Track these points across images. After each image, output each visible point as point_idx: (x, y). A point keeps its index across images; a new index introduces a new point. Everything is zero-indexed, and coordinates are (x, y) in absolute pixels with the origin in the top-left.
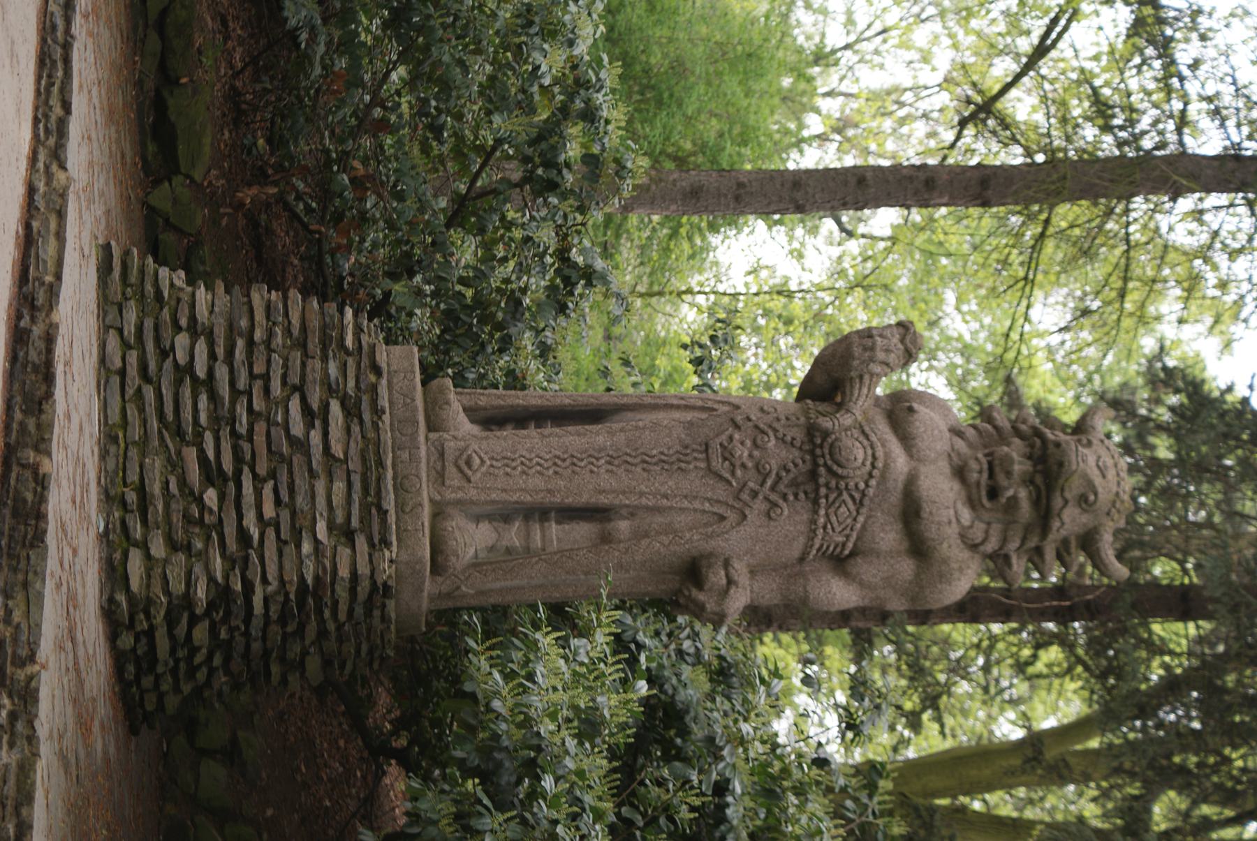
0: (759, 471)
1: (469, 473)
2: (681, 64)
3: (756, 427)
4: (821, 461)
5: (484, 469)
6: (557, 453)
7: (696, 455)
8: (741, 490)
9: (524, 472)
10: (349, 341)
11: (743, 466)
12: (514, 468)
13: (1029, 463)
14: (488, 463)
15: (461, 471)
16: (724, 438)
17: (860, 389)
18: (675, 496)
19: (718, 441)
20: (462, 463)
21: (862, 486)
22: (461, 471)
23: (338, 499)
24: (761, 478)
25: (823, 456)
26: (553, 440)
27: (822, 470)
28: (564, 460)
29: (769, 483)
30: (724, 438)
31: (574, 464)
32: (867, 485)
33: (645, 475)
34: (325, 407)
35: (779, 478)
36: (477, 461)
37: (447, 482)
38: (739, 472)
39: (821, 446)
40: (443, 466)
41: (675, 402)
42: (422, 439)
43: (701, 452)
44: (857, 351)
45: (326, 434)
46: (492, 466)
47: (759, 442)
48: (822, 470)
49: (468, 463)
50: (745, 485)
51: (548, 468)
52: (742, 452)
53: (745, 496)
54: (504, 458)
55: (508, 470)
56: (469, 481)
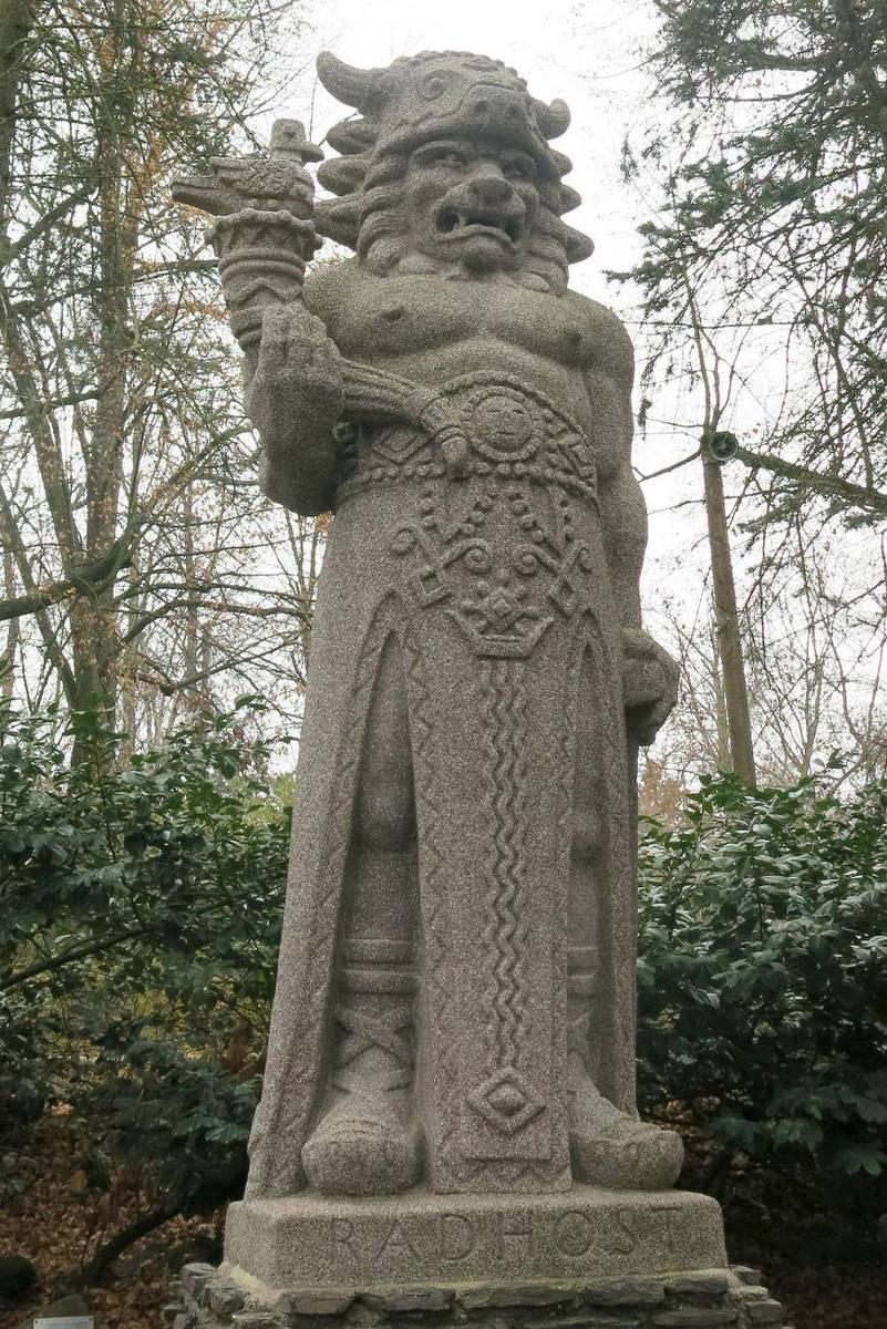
0: (531, 575)
3: (447, 566)
5: (522, 1079)
7: (501, 679)
8: (560, 611)
9: (524, 1001)
11: (522, 598)
12: (518, 1018)
13: (275, 137)
14: (509, 1070)
16: (472, 627)
17: (370, 385)
19: (477, 636)
20: (509, 1124)
24: (542, 573)
25: (513, 463)
26: (456, 939)
27: (533, 469)
28: (502, 921)
29: (549, 559)
30: (472, 627)
31: (510, 903)
32: (544, 404)
33: (530, 773)
35: (544, 542)
36: (506, 1092)
37: (545, 1153)
38: (532, 608)
39: (494, 463)
40: (511, 1160)
41: (362, 707)
42: (448, 1204)
43: (495, 668)
46: (514, 1063)
48: (533, 469)
49: (510, 1110)
50: (552, 601)
51: (517, 953)
52: (499, 598)
54: (498, 1038)
55: (521, 1029)
56: (542, 1110)
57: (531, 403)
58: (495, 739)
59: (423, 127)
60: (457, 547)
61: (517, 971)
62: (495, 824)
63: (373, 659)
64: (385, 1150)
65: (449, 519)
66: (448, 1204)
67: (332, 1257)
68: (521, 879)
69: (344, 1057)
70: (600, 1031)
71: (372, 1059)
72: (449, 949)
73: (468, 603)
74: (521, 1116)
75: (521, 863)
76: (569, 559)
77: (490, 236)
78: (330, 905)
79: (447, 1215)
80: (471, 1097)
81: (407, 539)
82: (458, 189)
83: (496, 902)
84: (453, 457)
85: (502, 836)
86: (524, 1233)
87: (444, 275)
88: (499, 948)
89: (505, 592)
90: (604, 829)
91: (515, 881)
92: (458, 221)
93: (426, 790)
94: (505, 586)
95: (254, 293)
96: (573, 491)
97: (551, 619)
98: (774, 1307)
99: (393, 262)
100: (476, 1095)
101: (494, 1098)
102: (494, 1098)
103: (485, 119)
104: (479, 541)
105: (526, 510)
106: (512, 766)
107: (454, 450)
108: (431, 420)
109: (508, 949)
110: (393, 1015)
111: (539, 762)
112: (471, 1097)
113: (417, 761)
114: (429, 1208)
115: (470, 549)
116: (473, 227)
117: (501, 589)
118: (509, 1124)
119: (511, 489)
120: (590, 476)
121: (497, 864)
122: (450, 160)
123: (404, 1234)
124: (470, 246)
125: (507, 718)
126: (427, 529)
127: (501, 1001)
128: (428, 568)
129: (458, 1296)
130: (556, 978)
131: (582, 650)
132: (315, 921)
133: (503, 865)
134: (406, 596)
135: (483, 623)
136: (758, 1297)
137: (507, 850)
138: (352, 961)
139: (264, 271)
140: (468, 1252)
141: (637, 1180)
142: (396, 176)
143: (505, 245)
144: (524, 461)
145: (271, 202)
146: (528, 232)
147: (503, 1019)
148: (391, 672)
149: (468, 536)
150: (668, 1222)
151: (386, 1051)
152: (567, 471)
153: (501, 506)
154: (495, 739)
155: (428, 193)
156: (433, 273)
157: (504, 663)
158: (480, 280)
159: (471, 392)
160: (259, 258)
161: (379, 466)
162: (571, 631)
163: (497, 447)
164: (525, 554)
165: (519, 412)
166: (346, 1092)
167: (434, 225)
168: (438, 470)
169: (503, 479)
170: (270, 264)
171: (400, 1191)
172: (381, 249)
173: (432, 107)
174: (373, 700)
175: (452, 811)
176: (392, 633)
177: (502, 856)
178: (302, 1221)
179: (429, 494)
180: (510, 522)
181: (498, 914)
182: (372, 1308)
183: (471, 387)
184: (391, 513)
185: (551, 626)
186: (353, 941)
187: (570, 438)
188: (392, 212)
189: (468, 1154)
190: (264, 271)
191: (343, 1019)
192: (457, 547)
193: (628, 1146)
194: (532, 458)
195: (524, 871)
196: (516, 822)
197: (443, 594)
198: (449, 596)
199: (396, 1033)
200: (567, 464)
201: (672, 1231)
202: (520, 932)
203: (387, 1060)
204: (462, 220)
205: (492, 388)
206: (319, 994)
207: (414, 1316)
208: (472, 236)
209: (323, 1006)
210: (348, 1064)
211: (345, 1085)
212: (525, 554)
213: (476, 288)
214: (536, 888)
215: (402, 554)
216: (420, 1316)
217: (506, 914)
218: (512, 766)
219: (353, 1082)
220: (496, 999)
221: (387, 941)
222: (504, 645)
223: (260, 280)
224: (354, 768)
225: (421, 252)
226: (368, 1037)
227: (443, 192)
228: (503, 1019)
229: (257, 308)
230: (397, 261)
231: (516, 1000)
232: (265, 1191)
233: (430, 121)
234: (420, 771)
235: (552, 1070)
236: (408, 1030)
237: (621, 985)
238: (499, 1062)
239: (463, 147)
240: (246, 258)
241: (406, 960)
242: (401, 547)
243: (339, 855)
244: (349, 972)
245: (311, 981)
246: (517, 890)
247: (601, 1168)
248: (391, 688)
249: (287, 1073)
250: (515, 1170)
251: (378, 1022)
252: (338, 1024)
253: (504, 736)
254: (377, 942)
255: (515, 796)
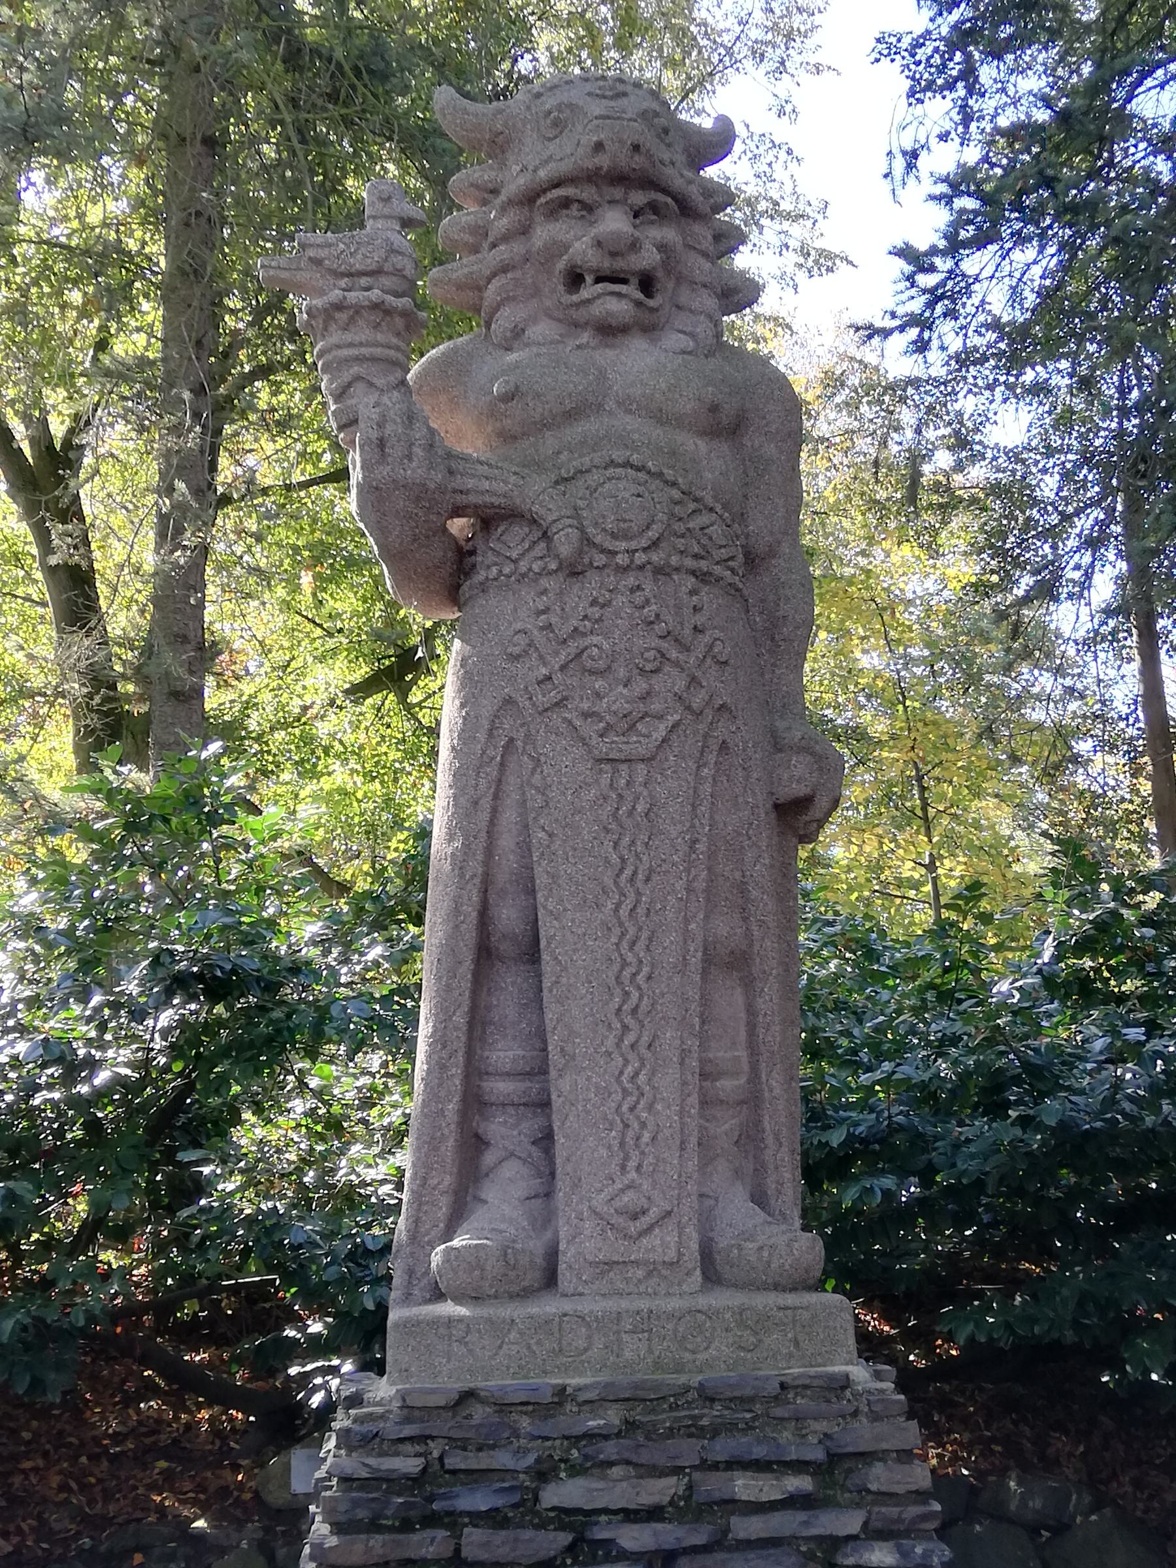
1: (654, 1213)
2: (509, 141)
3: (563, 668)
4: (640, 558)
6: (611, 1042)
9: (650, 1107)
10: (408, 1464)
11: (645, 697)
12: (643, 1125)
15: (650, 1229)
16: (589, 729)
17: (468, 492)
18: (693, 826)
20: (633, 1228)
21: (676, 494)
22: (650, 1229)
23: (767, 1488)
28: (626, 1028)
31: (634, 1011)
32: (674, 484)
33: (655, 878)
34: (565, 1517)
38: (656, 706)
40: (636, 1263)
41: (485, 816)
42: (567, 1306)
43: (616, 771)
44: (415, 471)
45: (630, 1516)
47: (601, 664)
51: (642, 1061)
53: (697, 702)
54: (622, 1144)
55: (646, 1137)
56: (669, 1213)
57: (655, 484)
58: (616, 844)
59: (542, 173)
60: (573, 646)
61: (642, 1078)
62: (617, 931)
63: (493, 771)
64: (506, 1254)
65: (565, 618)
66: (567, 1306)
67: (449, 1356)
68: (644, 986)
69: (484, 1168)
70: (750, 1139)
71: (510, 1169)
72: (573, 1057)
73: (585, 706)
74: (645, 1221)
75: (646, 970)
76: (699, 652)
77: (619, 295)
78: (460, 1019)
79: (565, 1315)
80: (594, 1202)
81: (522, 640)
82: (580, 242)
83: (619, 1010)
84: (565, 550)
85: (625, 944)
86: (643, 1331)
87: (571, 343)
88: (622, 1055)
89: (625, 691)
90: (748, 934)
91: (639, 988)
92: (584, 280)
93: (546, 900)
94: (626, 686)
95: (349, 385)
96: (703, 577)
97: (677, 717)
98: (898, 1402)
99: (518, 333)
100: (599, 1201)
101: (617, 1203)
102: (617, 1203)
103: (603, 161)
104: (596, 639)
105: (647, 601)
106: (635, 873)
107: (565, 543)
108: (542, 512)
109: (631, 1056)
110: (531, 1125)
111: (665, 867)
112: (594, 1202)
113: (538, 870)
114: (548, 1309)
115: (586, 648)
116: (600, 287)
117: (620, 688)
118: (633, 1228)
119: (631, 580)
120: (732, 558)
121: (621, 972)
122: (574, 210)
123: (521, 1333)
124: (597, 310)
125: (628, 823)
126: (542, 628)
127: (625, 1108)
128: (544, 671)
129: (569, 1390)
130: (685, 1083)
131: (716, 747)
132: (445, 1035)
133: (627, 973)
134: (523, 702)
135: (602, 725)
136: (882, 1391)
137: (630, 957)
138: (487, 1073)
139: (359, 359)
140: (586, 1350)
141: (770, 1281)
142: (525, 231)
143: (639, 304)
144: (645, 550)
145: (364, 281)
146: (670, 285)
147: (627, 1126)
148: (512, 782)
149: (584, 635)
150: (794, 1321)
151: (525, 1161)
152: (696, 556)
153: (620, 600)
154: (616, 844)
155: (558, 248)
156: (559, 342)
157: (624, 767)
158: (612, 346)
159: (588, 476)
160: (351, 345)
161: (496, 564)
162: (702, 727)
163: (614, 536)
164: (648, 650)
165: (639, 496)
166: (485, 1202)
167: (561, 288)
168: (553, 566)
169: (626, 569)
170: (365, 351)
171: (525, 1294)
172: (505, 319)
173: (552, 147)
174: (494, 811)
175: (573, 921)
176: (511, 740)
177: (625, 964)
178: (419, 1323)
179: (545, 592)
180: (631, 616)
181: (621, 1021)
182: (484, 1402)
183: (587, 471)
184: (511, 611)
185: (676, 725)
186: (486, 1053)
187: (704, 519)
188: (518, 274)
189: (590, 1258)
190: (359, 359)
191: (480, 1131)
192: (573, 646)
193: (761, 1248)
194: (655, 544)
195: (649, 978)
196: (640, 929)
197: (559, 697)
198: (566, 698)
199: (533, 1143)
200: (696, 549)
201: (798, 1329)
202: (645, 1039)
203: (525, 1171)
204: (589, 279)
205: (610, 472)
206: (452, 1107)
207: (524, 1408)
208: (599, 296)
209: (456, 1118)
210: (487, 1175)
211: (483, 1196)
212: (648, 650)
213: (605, 356)
214: (663, 995)
215: (515, 658)
216: (530, 1408)
217: (628, 1020)
218: (635, 873)
219: (490, 1192)
220: (620, 1106)
221: (521, 1053)
222: (624, 747)
223: (356, 369)
224: (477, 881)
225: (551, 317)
226: (506, 1149)
227: (566, 247)
228: (627, 1126)
229: (353, 401)
230: (523, 330)
231: (640, 1106)
232: (407, 1299)
233: (552, 165)
234: (541, 880)
235: (680, 1176)
236: (546, 1140)
237: (771, 1091)
238: (623, 1168)
239: (587, 193)
240: (338, 347)
241: (539, 1070)
242: (516, 650)
243: (468, 965)
244: (484, 1084)
245: (442, 1094)
246: (641, 998)
247: (735, 1270)
248: (512, 797)
249: (423, 1185)
250: (640, 1273)
251: (515, 1133)
252: (477, 1136)
253: (626, 840)
254: (510, 1054)
255: (638, 901)
